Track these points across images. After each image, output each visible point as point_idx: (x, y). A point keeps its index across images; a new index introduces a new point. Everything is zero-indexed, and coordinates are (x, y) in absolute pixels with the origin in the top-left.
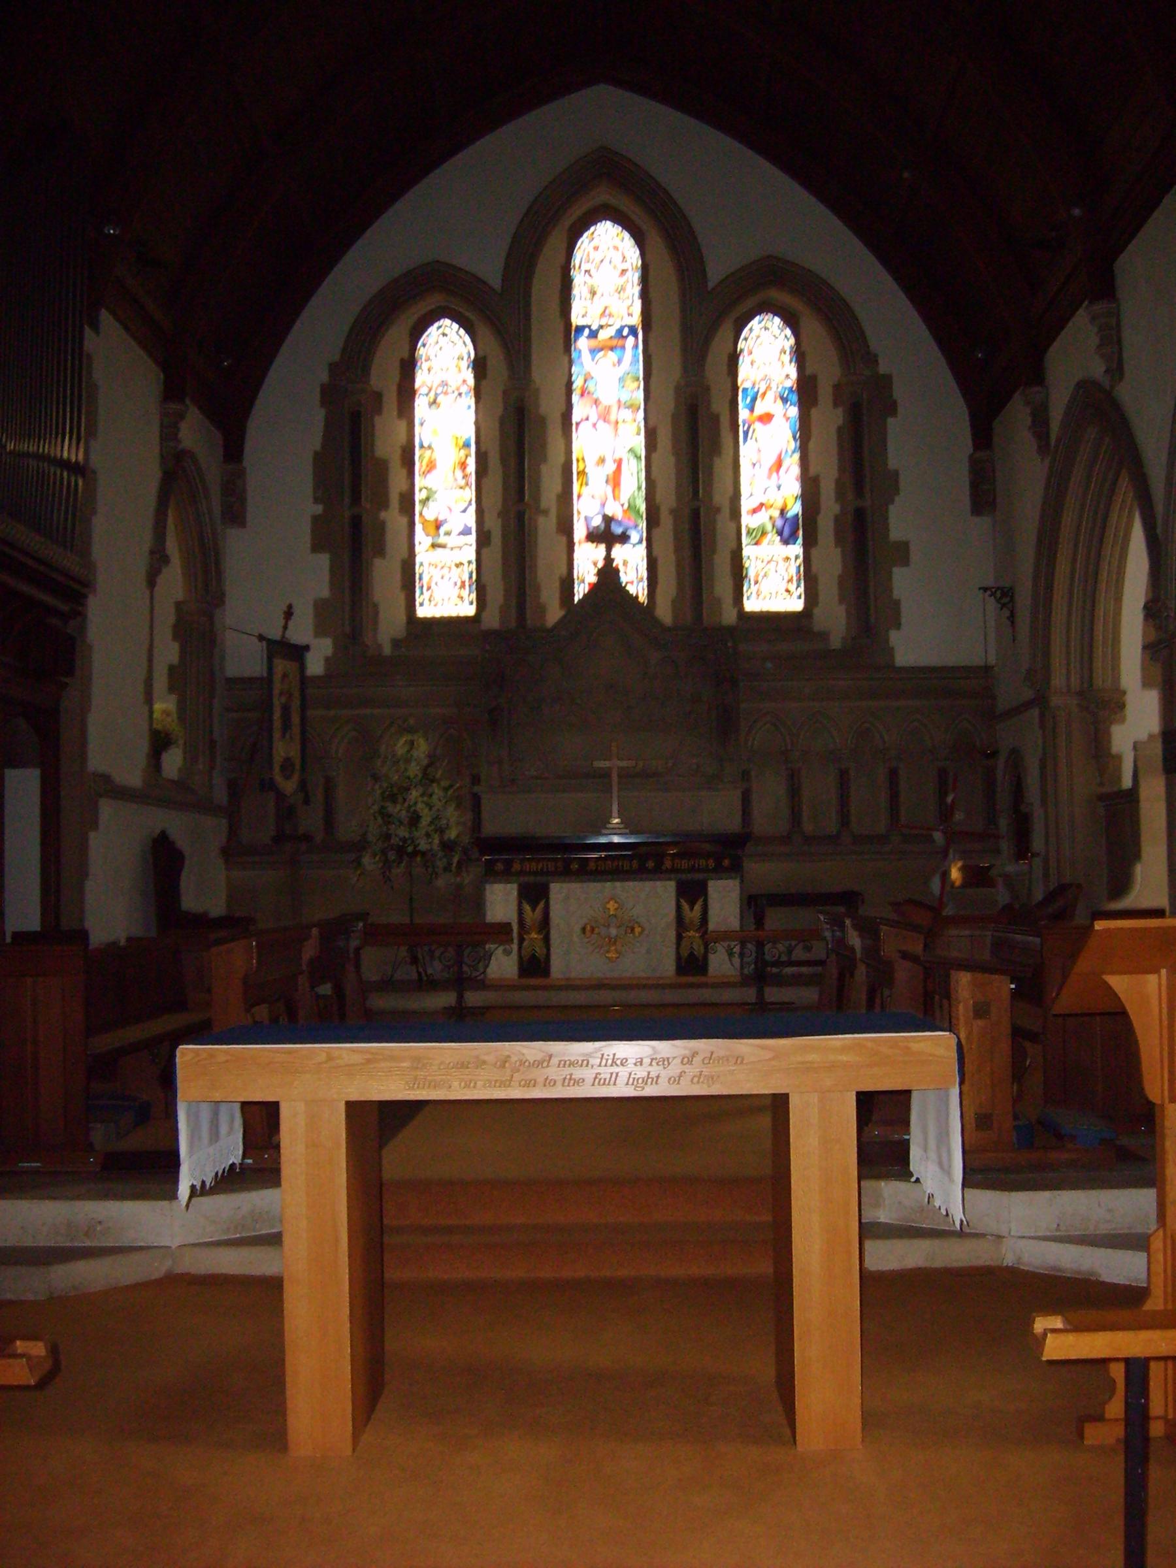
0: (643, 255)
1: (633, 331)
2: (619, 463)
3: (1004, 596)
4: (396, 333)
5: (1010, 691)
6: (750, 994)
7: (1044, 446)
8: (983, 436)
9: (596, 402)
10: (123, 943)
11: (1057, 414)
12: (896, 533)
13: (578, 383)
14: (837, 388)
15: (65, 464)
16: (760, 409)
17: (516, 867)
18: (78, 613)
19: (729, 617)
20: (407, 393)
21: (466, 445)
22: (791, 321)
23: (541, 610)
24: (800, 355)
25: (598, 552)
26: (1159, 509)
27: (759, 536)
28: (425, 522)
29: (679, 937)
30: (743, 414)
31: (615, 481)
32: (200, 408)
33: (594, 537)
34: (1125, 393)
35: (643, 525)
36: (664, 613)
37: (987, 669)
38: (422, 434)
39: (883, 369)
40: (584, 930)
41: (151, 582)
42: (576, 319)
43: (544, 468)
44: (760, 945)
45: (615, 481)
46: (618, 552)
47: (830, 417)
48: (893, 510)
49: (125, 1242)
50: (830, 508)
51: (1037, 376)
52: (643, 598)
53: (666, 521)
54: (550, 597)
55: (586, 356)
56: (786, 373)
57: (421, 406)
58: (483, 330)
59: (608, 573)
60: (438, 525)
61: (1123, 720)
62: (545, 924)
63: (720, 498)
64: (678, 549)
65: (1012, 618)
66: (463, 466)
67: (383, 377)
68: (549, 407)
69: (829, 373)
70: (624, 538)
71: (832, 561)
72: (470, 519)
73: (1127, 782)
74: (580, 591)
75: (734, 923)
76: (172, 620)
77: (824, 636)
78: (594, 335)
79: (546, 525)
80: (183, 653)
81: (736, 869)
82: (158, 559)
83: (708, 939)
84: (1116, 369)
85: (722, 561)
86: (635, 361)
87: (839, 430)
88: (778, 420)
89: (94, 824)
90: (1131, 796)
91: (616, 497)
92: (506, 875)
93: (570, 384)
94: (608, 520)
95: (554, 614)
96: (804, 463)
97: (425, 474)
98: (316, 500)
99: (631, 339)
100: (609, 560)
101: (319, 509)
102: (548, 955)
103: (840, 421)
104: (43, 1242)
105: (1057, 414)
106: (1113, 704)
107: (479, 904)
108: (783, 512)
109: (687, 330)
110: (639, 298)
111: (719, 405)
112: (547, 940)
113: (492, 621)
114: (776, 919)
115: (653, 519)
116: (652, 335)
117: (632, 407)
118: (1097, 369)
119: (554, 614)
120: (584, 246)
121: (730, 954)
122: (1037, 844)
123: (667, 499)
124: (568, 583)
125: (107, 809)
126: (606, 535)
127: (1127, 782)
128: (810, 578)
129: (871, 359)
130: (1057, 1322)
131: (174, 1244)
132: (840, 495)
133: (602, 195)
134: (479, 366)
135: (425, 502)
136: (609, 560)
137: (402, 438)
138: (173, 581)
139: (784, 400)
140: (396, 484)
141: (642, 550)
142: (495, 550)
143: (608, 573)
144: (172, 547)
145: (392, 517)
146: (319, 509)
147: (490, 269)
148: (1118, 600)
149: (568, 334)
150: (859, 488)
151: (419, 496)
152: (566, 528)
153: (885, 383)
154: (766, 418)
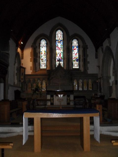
0: (63, 33)
1: (62, 40)
2: (60, 53)
3: (99, 67)
4: (39, 40)
5: (99, 76)
6: (74, 106)
7: (103, 52)
8: (96, 51)
9: (58, 47)
10: (11, 101)
11: (104, 49)
12: (88, 60)
13: (57, 45)
14: (82, 46)
15: (7, 53)
16: (74, 48)
17: (50, 93)
18: (8, 68)
19: (71, 69)
20: (40, 46)
21: (45, 52)
22: (78, 40)
23: (53, 68)
24: (78, 43)
25: (59, 62)
26: (115, 57)
27: (74, 61)
28: (41, 59)
29: (67, 101)
30: (73, 49)
31: (60, 55)
32: (20, 48)
33: (58, 61)
34: (111, 47)
35: (63, 60)
36: (65, 68)
37: (97, 74)
38: (41, 50)
39: (87, 44)
40: (57, 100)
41: (14, 65)
42: (56, 39)
43: (53, 54)
44: (75, 101)
45: (60, 55)
46: (61, 62)
47: (81, 49)
48: (88, 58)
49: (12, 131)
50: (81, 58)
51: (102, 45)
52: (62, 66)
53: (65, 59)
54: (54, 66)
55: (57, 43)
56: (77, 45)
57: (41, 48)
58: (47, 40)
59: (60, 64)
60: (43, 59)
61: (111, 79)
62: (53, 99)
63: (71, 57)
64: (67, 62)
65: (100, 69)
66: (45, 53)
67: (37, 45)
68: (54, 48)
69: (81, 44)
70: (61, 61)
71: (82, 63)
72: (46, 59)
73: (111, 85)
74: (57, 66)
75: (73, 99)
76: (16, 68)
77: (81, 71)
78: (58, 41)
79: (53, 60)
80: (17, 72)
81: (73, 94)
82: (15, 62)
83: (70, 101)
84: (110, 45)
85: (71, 63)
86: (62, 44)
87: (82, 50)
88: (76, 49)
89: (9, 89)
90: (112, 87)
91: (60, 57)
92: (49, 94)
93: (56, 45)
94: (59, 59)
95: (54, 68)
96: (79, 54)
97: (41, 54)
98: (31, 57)
99: (62, 42)
100: (59, 63)
101: (31, 58)
102: (53, 103)
103: (82, 49)
104: (6, 131)
105: (104, 49)
106: (109, 78)
107: (46, 97)
108: (77, 58)
109: (67, 40)
110: (31, 61)
111: (70, 48)
112: (53, 101)
113: (48, 69)
114: (76, 99)
115: (64, 59)
116: (64, 41)
117: (62, 48)
118: (108, 45)
119: (54, 68)
120: (57, 32)
121: (72, 102)
122: (102, 91)
123: (65, 57)
124: (55, 65)
125: (10, 87)
126: (59, 60)
127: (111, 85)
128: (79, 65)
129: (86, 43)
130: (114, 141)
131: (19, 132)
132: (82, 57)
133: (59, 27)
134: (47, 44)
135: (41, 57)
136: (59, 63)
137: (39, 51)
138: (16, 65)
139: (77, 47)
140: (38, 55)
141: (63, 62)
142: (48, 62)
143: (60, 64)
144: (17, 61)
145: (38, 59)
146: (31, 58)
147: (48, 34)
148: (110, 67)
149: (56, 41)
150: (84, 56)
151: (41, 56)
152: (55, 60)
153: (87, 46)
154: (75, 49)
